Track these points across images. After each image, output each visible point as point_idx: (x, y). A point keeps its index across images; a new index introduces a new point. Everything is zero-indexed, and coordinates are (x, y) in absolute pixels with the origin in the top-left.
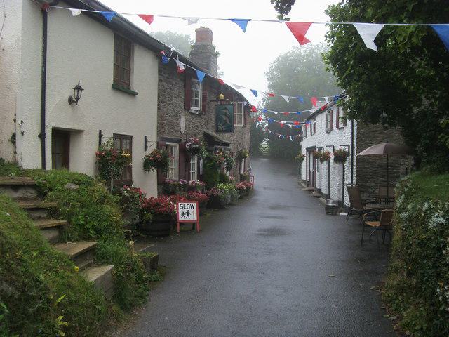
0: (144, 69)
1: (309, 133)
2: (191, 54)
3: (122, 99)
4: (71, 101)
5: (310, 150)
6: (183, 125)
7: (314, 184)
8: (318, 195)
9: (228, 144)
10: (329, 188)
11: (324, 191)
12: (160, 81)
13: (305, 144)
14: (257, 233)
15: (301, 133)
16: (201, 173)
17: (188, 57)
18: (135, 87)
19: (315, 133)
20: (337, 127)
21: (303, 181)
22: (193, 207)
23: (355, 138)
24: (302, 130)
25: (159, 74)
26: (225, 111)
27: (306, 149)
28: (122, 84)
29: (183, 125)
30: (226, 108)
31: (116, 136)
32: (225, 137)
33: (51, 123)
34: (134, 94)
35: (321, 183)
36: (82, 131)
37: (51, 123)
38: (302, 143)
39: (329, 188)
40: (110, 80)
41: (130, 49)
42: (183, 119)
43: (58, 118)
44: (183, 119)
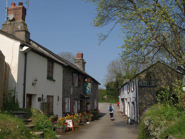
0: (58, 72)
3: (50, 82)
4: (33, 84)
6: (72, 91)
7: (124, 113)
12: (64, 75)
14: (16, 99)
16: (79, 109)
18: (54, 78)
20: (131, 91)
22: (70, 122)
23: (137, 91)
25: (101, 102)
28: (50, 78)
29: (72, 91)
31: (48, 96)
33: (27, 92)
34: (54, 81)
36: (36, 95)
37: (27, 92)
40: (46, 77)
42: (72, 89)
43: (30, 90)
44: (72, 89)
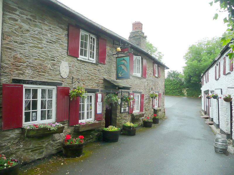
1: (205, 82)
2: (130, 37)
5: (207, 92)
8: (211, 122)
9: (128, 88)
10: (219, 119)
11: (216, 121)
13: (203, 89)
15: (201, 82)
17: (128, 39)
19: (208, 81)
20: (224, 74)
21: (203, 111)
24: (202, 81)
26: (123, 62)
27: (204, 92)
30: (124, 60)
32: (122, 83)
35: (213, 114)
38: (201, 89)
39: (219, 119)
41: (140, 51)
